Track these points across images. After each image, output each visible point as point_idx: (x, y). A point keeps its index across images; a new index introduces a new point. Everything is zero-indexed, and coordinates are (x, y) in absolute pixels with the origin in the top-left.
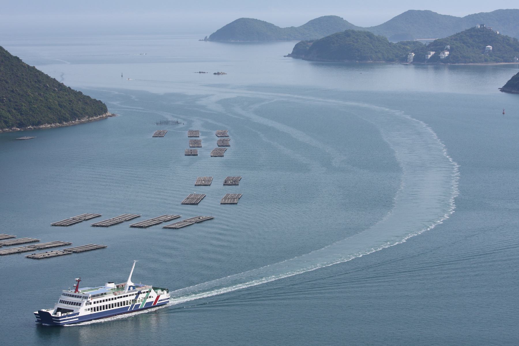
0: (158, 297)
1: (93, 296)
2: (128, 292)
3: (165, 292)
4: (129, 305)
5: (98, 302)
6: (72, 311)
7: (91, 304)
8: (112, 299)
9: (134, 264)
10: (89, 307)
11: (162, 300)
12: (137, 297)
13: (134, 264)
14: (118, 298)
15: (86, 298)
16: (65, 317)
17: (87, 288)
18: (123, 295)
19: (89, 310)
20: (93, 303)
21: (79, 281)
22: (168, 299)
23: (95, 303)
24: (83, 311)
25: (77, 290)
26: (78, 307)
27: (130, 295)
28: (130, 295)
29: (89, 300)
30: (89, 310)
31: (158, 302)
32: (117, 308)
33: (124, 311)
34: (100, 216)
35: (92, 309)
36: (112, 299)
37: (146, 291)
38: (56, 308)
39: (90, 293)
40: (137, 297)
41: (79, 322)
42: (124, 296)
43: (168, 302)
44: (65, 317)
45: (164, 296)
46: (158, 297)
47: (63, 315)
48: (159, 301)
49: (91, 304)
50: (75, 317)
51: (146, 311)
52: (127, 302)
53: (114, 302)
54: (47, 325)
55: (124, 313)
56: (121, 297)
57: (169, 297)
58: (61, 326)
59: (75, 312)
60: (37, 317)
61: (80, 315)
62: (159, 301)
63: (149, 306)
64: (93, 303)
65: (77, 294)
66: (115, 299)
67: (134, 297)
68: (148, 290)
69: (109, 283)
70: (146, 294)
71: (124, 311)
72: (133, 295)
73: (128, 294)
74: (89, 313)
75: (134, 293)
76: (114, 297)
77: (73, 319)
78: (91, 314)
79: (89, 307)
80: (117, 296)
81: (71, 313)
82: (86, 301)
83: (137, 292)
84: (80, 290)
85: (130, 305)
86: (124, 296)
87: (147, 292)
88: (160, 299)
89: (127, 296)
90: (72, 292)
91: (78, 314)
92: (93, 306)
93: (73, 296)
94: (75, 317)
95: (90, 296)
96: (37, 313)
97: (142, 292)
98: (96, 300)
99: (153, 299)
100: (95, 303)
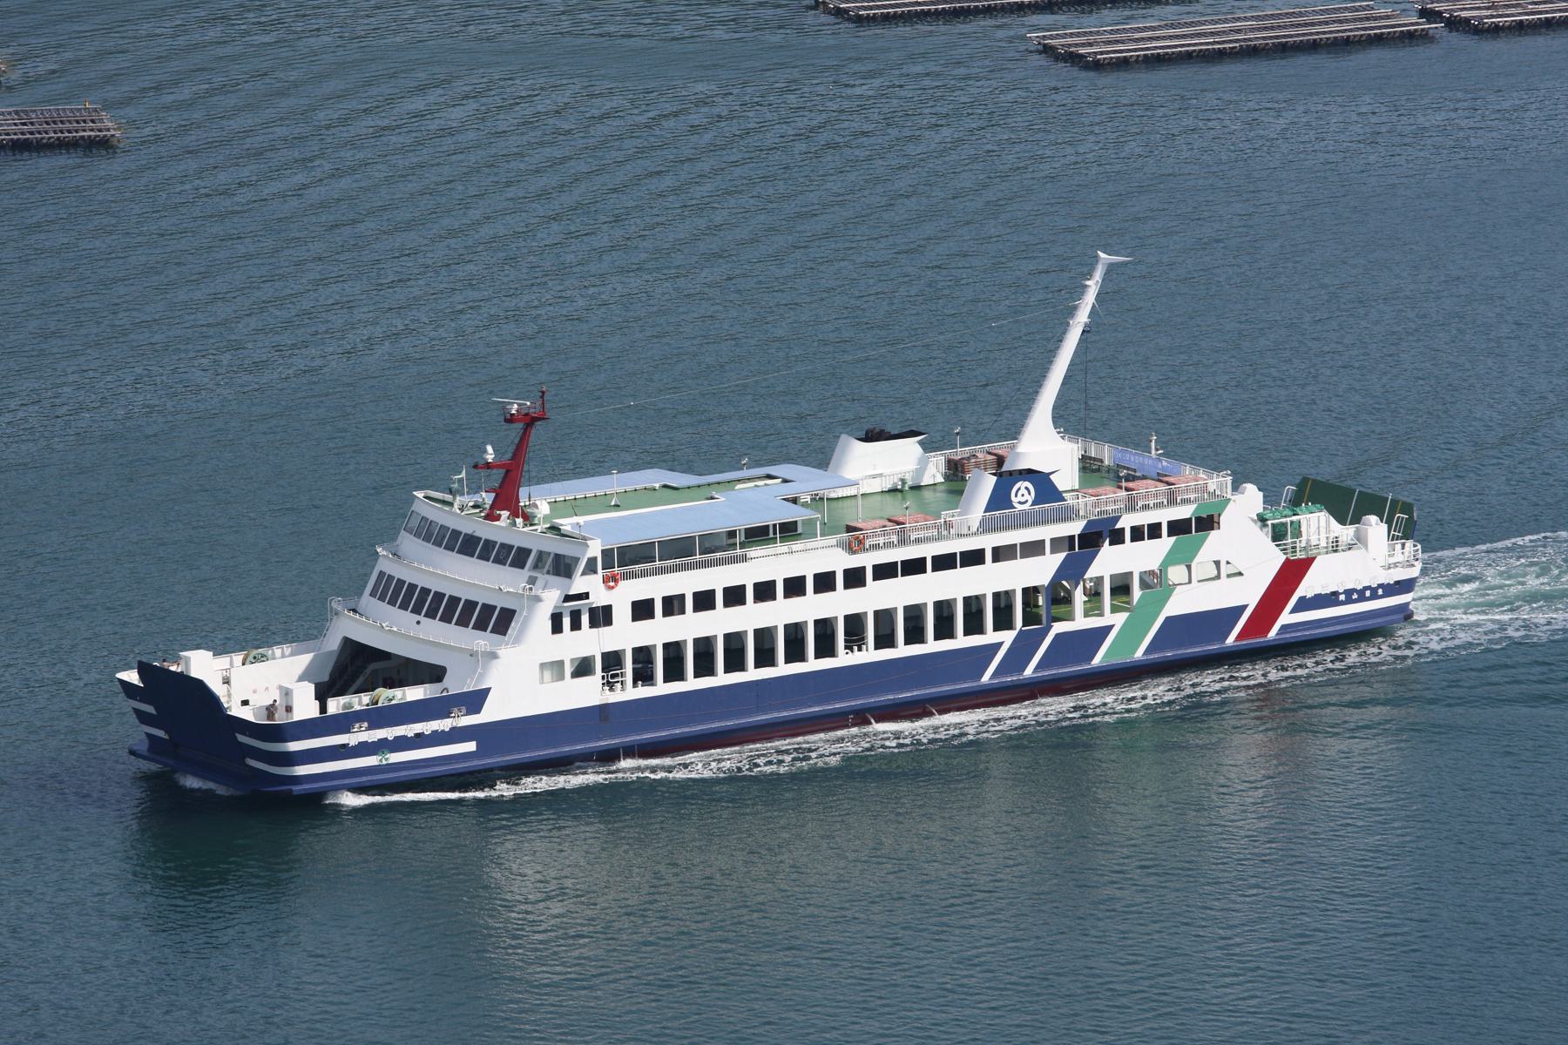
0: (1293, 572)
1: (628, 558)
2: (987, 527)
3: (1375, 528)
4: (990, 637)
5: (673, 605)
6: (435, 674)
7: (602, 617)
8: (825, 582)
9: (1093, 286)
10: (590, 642)
11: (1330, 599)
12: (1073, 569)
13: (1093, 286)
14: (884, 571)
15: (563, 567)
16: (343, 723)
17: (655, 477)
18: (928, 551)
19: (583, 668)
20: (622, 613)
21: (529, 421)
22: (1404, 586)
23: (642, 610)
24: (524, 679)
25: (506, 499)
26: (481, 641)
27: (1000, 554)
28: (1000, 554)
29: (579, 584)
30: (583, 668)
31: (1286, 618)
32: (870, 654)
33: (952, 686)
34: (102, 145)
35: (612, 661)
36: (825, 582)
37: (1164, 516)
38: (333, 643)
39: (596, 533)
40: (1073, 569)
41: (483, 778)
42: (944, 563)
43: (1404, 613)
44: (343, 723)
45: (1358, 560)
46: (1293, 572)
47: (335, 706)
48: (1304, 605)
49: (602, 617)
50: (444, 725)
51: (1157, 691)
52: (576, 625)
53: (839, 604)
54: (217, 800)
55: (947, 704)
56: (914, 567)
57: (1415, 572)
58: (311, 804)
59: (454, 684)
60: (142, 717)
61: (490, 713)
62: (1304, 605)
63: (1194, 644)
64: (622, 613)
65: (503, 529)
66: (855, 578)
67: (1041, 571)
68: (1184, 512)
69: (871, 436)
70: (1166, 542)
71: (952, 686)
72: (1154, 531)
73: (988, 542)
74: (589, 693)
75: (1046, 533)
76: (838, 561)
77: (420, 741)
78: (603, 710)
79: (590, 642)
80: (867, 560)
81: (415, 693)
82: (551, 598)
83: (1075, 528)
84: (540, 500)
85: (1007, 637)
86: (944, 563)
87: (1177, 528)
88: (1310, 585)
89: (973, 558)
90: (464, 511)
91: (475, 700)
92: (625, 635)
93: (469, 546)
94: (444, 725)
95: (595, 549)
96: (132, 677)
97: (1126, 522)
98: (656, 587)
99: (1248, 593)
100: (642, 610)
